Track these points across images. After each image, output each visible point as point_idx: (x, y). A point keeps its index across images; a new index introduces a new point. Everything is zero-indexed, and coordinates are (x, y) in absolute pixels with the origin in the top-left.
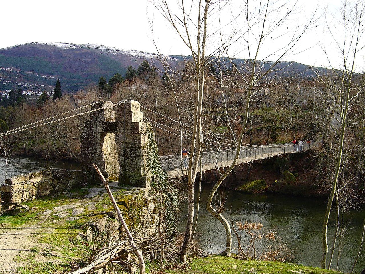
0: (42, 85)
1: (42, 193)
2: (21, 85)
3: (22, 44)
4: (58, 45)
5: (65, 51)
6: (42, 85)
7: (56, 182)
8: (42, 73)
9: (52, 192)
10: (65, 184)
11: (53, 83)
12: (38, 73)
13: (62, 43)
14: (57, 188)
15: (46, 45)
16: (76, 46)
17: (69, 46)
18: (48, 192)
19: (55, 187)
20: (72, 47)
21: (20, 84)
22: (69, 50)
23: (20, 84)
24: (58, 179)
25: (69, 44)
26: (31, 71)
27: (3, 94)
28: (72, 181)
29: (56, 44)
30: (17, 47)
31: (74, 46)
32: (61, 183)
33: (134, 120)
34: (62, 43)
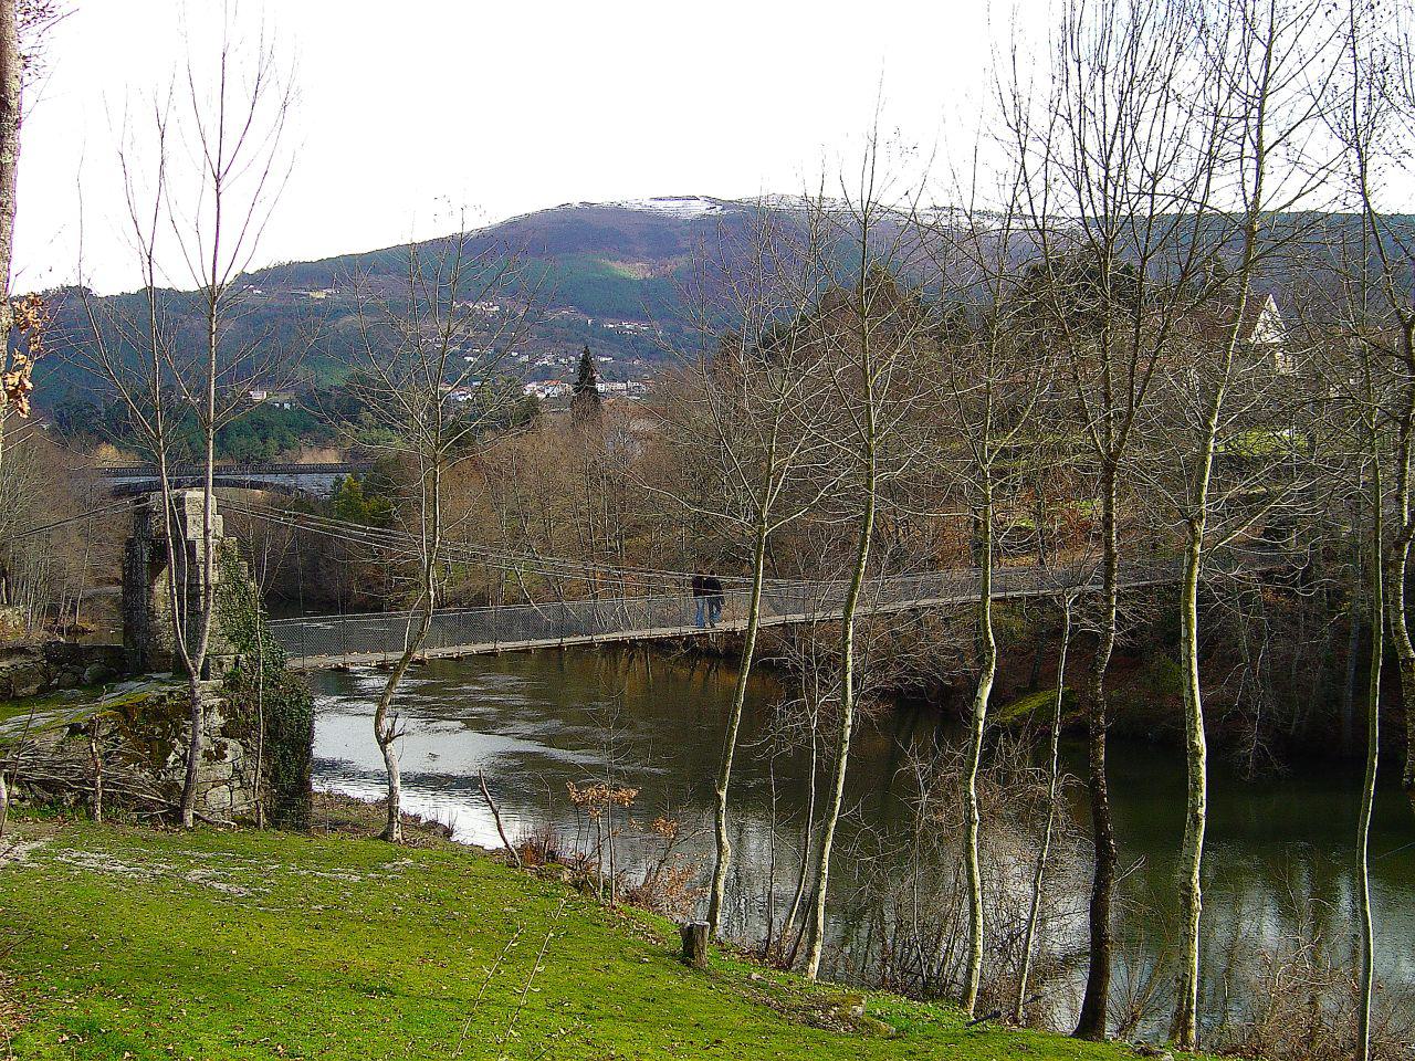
0: (604, 359)
1: (18, 691)
2: (531, 362)
3: (530, 211)
4: (660, 205)
5: (688, 228)
6: (604, 359)
7: (53, 668)
8: (604, 314)
9: (41, 690)
10: (74, 674)
11: (644, 349)
12: (591, 315)
13: (677, 198)
14: (55, 682)
15: (618, 211)
16: (727, 204)
17: (699, 208)
18: (33, 689)
19: (50, 680)
20: (713, 212)
21: (525, 358)
22: (701, 222)
23: (525, 358)
24: (59, 662)
25: (702, 199)
26: (566, 308)
27: (460, 400)
28: (95, 666)
29: (653, 202)
30: (512, 224)
31: (718, 208)
32: (66, 670)
33: (190, 536)
34: (677, 198)
